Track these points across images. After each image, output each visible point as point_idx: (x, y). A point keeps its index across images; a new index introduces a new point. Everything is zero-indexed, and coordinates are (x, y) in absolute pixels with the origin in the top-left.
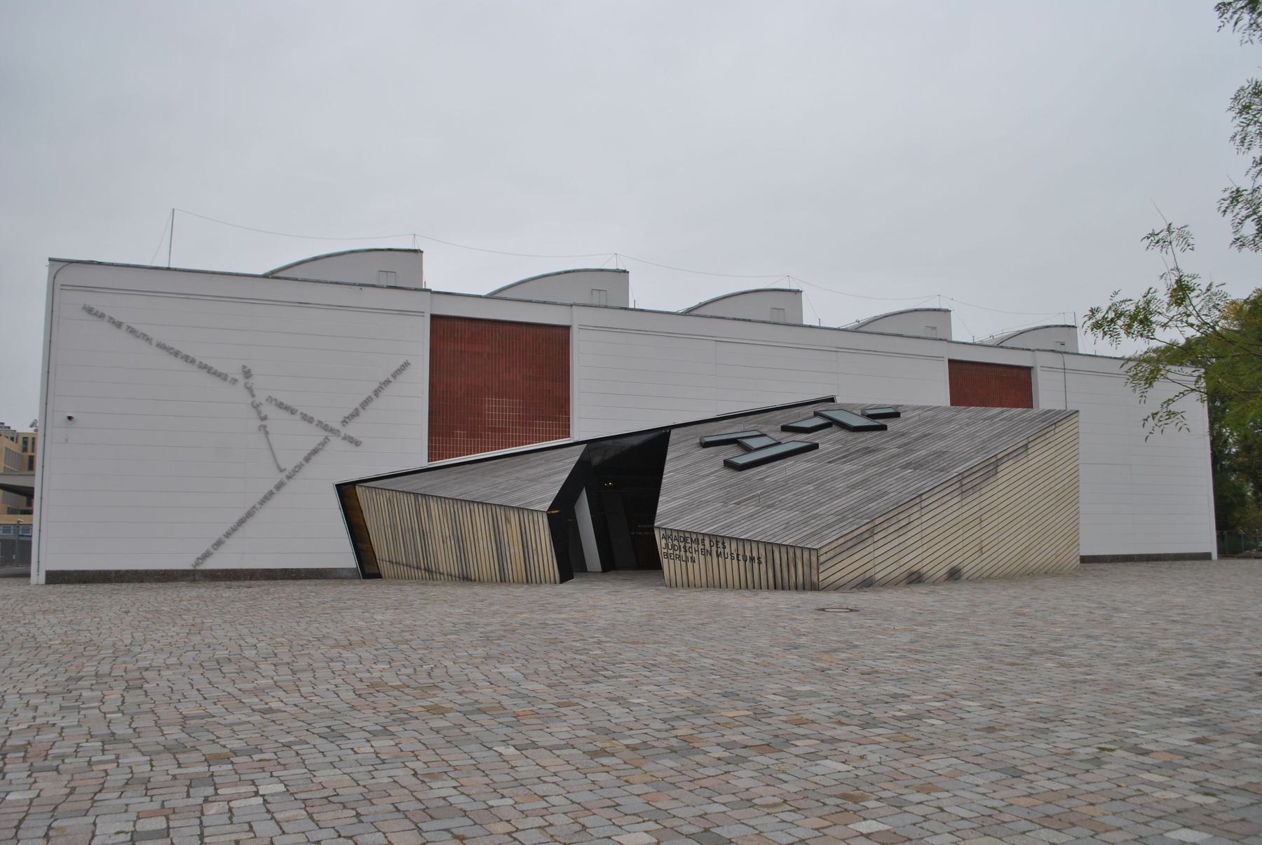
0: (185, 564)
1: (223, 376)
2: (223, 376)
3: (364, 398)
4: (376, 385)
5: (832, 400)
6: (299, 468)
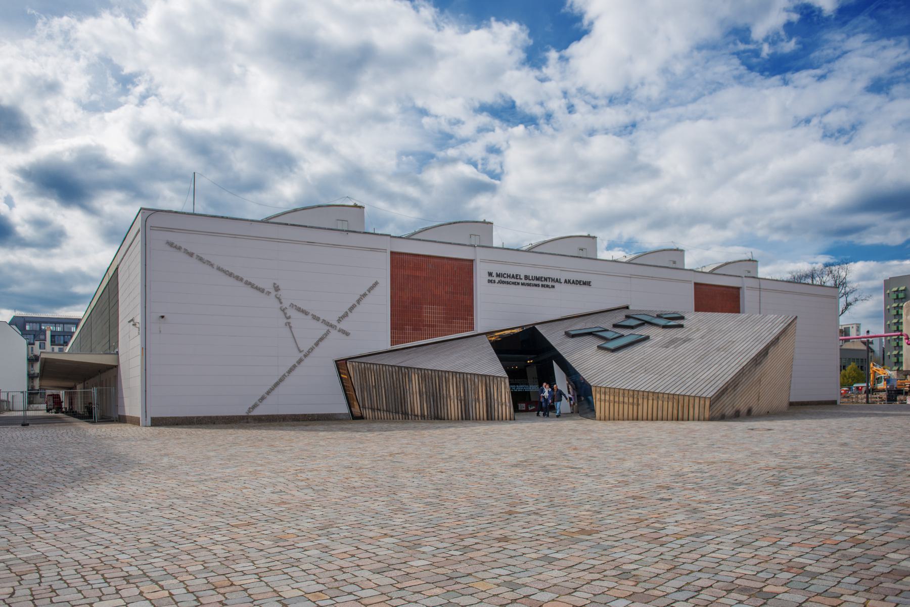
0: (242, 411)
1: (262, 290)
2: (262, 290)
3: (351, 305)
4: (358, 297)
5: (627, 308)
6: (312, 349)
